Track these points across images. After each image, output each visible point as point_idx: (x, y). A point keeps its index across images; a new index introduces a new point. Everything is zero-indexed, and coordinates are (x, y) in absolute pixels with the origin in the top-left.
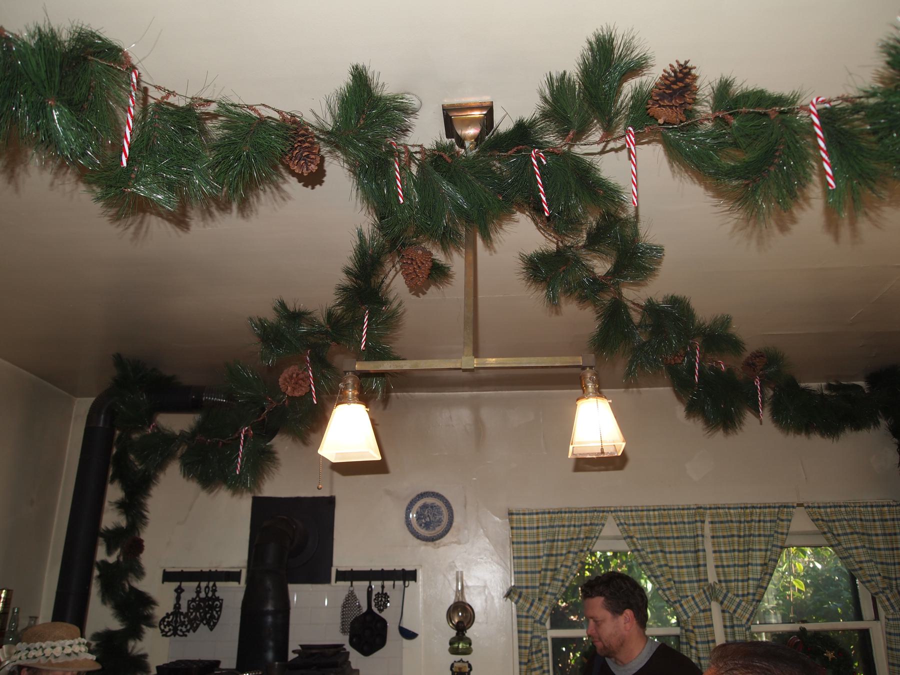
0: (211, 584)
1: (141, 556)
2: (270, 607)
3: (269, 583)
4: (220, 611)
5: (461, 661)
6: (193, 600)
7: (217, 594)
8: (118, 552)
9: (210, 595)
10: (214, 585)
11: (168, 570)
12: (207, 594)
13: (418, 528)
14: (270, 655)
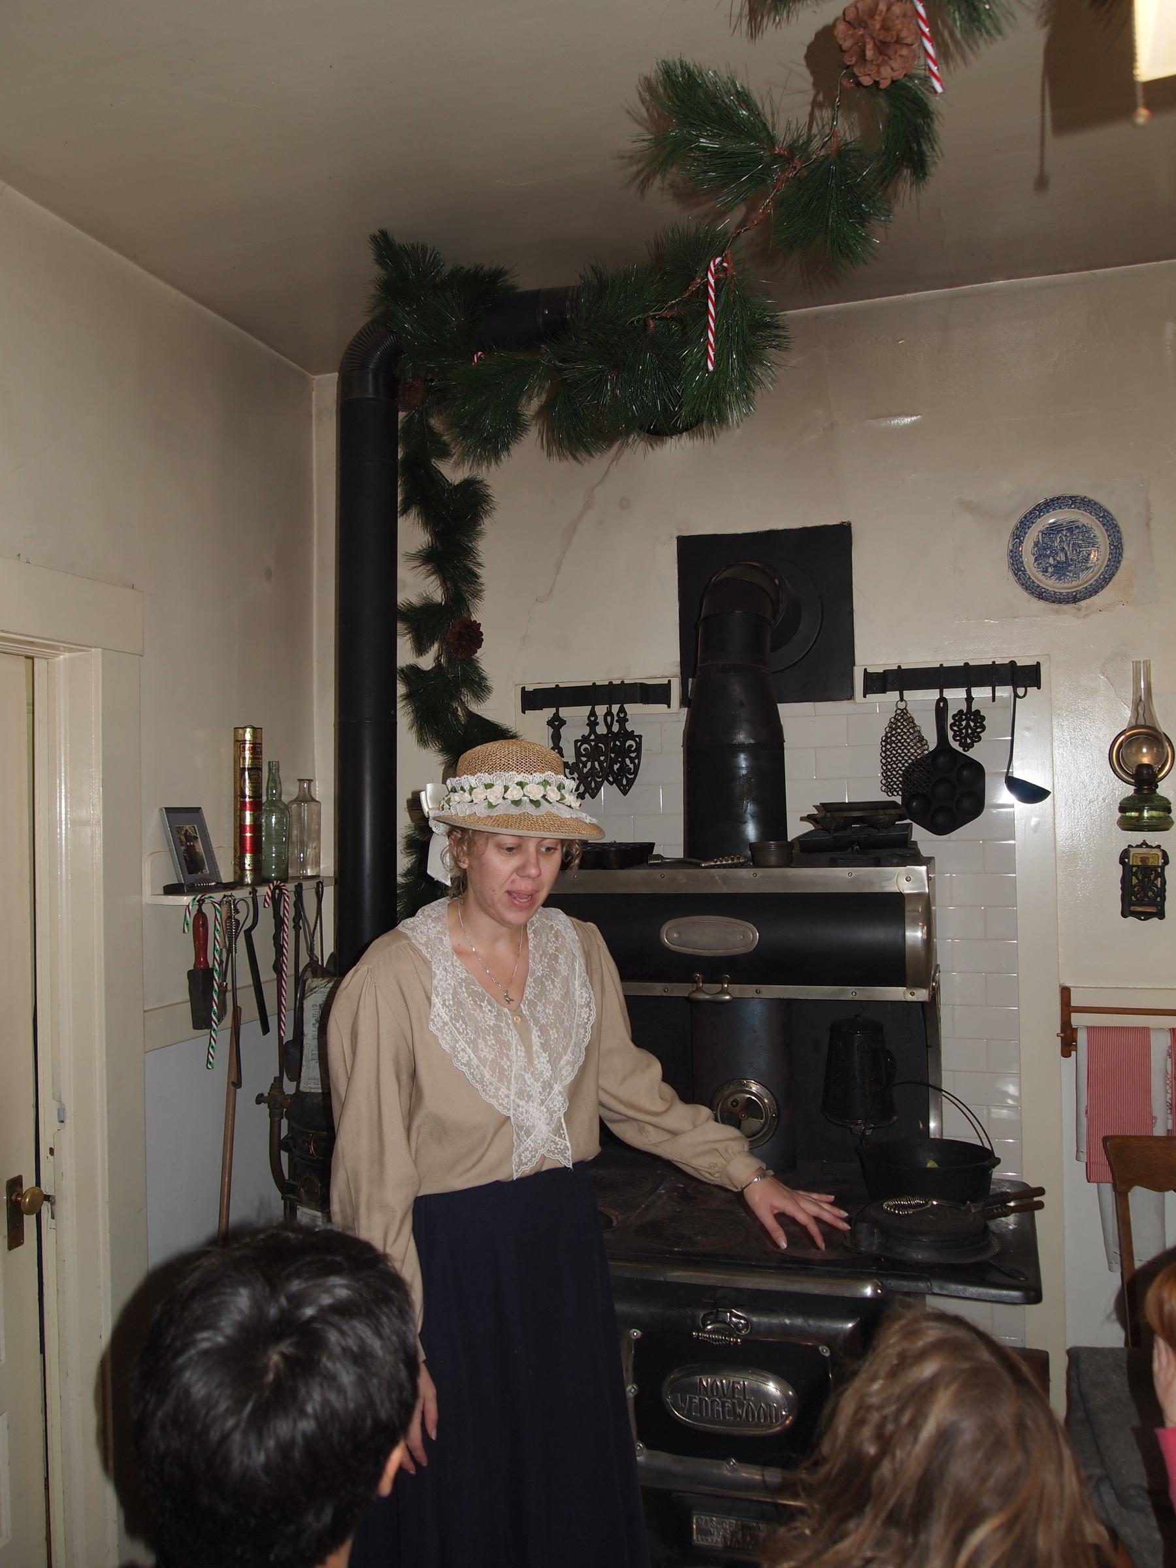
0: (615, 708)
1: (480, 653)
2: (742, 737)
3: (737, 690)
4: (639, 757)
5: (1144, 844)
6: (585, 739)
7: (629, 727)
8: (435, 649)
9: (616, 728)
10: (622, 710)
11: (529, 688)
12: (609, 727)
13: (1040, 575)
14: (751, 831)
